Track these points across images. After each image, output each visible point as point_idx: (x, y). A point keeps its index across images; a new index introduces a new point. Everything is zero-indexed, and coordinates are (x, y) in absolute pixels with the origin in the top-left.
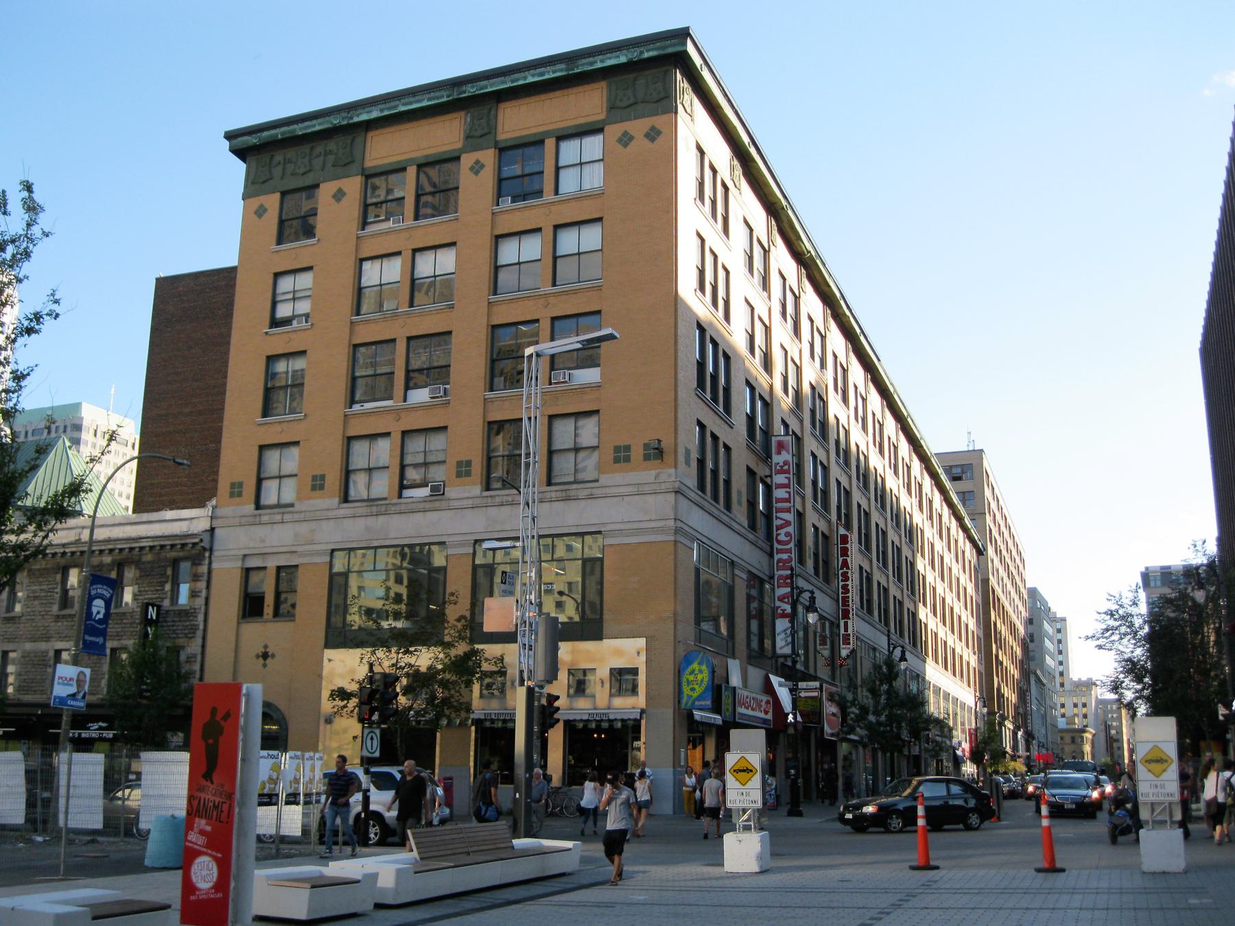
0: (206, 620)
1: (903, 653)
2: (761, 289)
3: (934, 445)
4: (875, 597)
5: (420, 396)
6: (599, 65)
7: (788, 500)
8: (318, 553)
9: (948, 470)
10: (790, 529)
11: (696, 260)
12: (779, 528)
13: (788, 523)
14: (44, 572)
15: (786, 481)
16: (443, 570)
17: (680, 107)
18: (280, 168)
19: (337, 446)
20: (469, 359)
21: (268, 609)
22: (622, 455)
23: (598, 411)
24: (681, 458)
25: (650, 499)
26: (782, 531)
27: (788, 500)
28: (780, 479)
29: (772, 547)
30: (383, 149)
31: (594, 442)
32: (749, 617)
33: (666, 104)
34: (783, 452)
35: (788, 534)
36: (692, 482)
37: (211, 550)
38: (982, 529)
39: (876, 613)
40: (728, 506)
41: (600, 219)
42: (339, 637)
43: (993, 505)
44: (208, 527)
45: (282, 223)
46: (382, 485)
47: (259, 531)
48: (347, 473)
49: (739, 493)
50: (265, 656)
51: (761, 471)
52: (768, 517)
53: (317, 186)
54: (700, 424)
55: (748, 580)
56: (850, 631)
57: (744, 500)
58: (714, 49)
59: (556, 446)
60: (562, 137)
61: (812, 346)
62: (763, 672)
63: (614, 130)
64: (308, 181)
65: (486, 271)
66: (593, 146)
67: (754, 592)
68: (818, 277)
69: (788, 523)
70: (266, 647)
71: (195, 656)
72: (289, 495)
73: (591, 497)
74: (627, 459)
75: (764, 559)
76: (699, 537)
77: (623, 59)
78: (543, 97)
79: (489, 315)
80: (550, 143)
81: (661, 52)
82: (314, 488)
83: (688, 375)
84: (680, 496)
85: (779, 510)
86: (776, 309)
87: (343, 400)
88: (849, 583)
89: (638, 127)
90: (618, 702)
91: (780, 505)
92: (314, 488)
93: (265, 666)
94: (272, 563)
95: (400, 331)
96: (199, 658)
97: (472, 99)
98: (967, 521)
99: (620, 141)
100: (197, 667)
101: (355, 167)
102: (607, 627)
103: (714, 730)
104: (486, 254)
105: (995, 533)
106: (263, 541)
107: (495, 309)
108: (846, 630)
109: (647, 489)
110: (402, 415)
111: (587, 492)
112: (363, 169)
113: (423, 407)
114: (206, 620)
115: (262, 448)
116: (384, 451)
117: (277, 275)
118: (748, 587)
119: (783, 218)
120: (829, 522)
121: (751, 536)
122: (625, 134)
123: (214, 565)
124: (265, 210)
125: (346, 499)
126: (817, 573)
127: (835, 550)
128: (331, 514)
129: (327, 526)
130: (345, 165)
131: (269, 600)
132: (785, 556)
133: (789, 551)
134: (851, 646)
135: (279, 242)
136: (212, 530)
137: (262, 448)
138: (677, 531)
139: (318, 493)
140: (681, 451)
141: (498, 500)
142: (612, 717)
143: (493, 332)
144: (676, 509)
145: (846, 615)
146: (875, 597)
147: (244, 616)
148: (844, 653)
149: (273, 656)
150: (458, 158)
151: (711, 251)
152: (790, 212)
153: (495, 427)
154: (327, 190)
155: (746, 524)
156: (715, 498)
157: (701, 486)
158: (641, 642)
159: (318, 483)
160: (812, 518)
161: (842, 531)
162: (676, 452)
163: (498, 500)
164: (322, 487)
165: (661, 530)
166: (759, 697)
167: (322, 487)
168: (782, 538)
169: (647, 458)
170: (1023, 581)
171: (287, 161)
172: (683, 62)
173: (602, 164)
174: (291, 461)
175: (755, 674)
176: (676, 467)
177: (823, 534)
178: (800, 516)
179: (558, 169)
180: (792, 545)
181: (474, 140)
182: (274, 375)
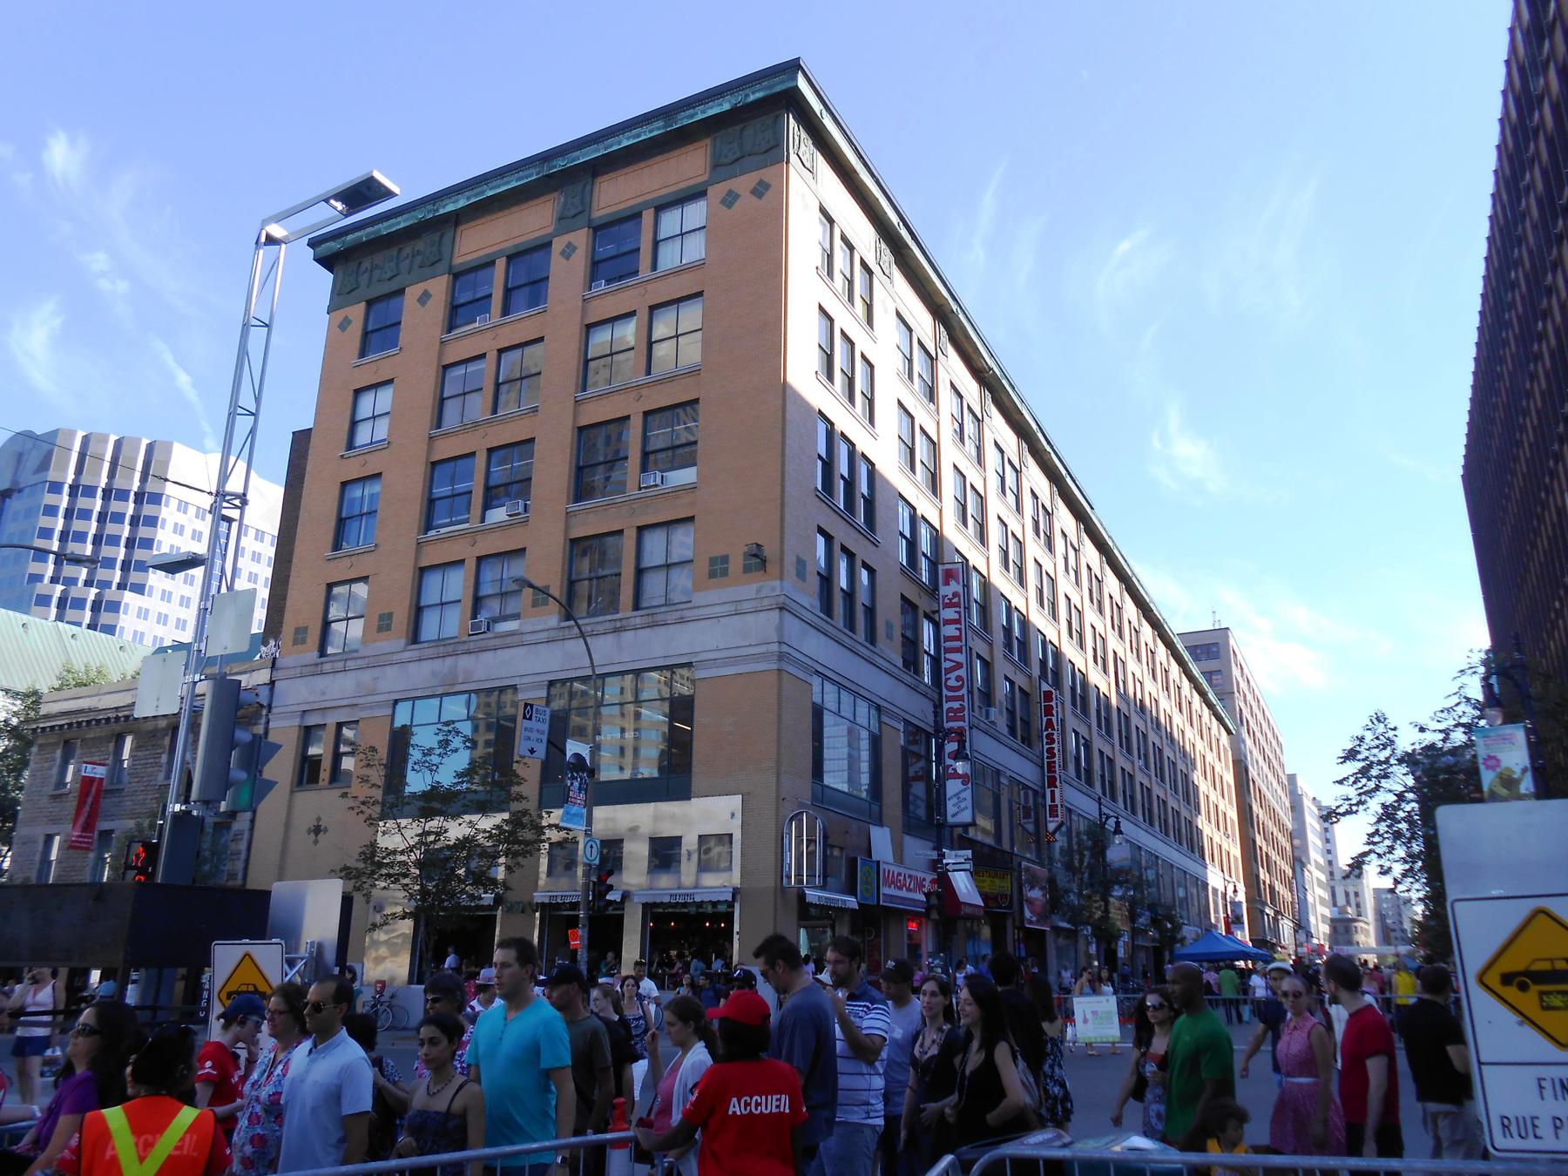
1: (1118, 823)
2: (925, 401)
3: (1177, 625)
4: (1139, 797)
5: (498, 515)
6: (700, 117)
7: (958, 638)
8: (379, 705)
9: (1192, 649)
10: (962, 672)
12: (948, 671)
13: (959, 666)
14: (97, 741)
17: (793, 158)
19: (406, 577)
20: (552, 469)
21: (325, 775)
22: (718, 568)
26: (953, 675)
27: (958, 638)
28: (949, 614)
29: (940, 694)
30: (473, 243)
33: (775, 153)
34: (953, 583)
35: (959, 678)
36: (808, 598)
37: (270, 707)
38: (1231, 709)
39: (1140, 812)
40: (872, 638)
41: (700, 294)
42: (394, 802)
43: (1243, 685)
44: (267, 680)
46: (453, 623)
47: (321, 682)
48: (418, 611)
49: (889, 625)
50: (317, 830)
51: (924, 604)
53: (401, 292)
56: (1058, 802)
58: (830, 84)
59: (646, 563)
60: (661, 207)
61: (1066, 559)
63: (717, 191)
64: (394, 285)
66: (696, 213)
68: (1007, 403)
69: (959, 666)
70: (319, 819)
71: (241, 833)
73: (682, 621)
74: (725, 573)
77: (726, 107)
78: (642, 164)
79: (575, 416)
80: (648, 216)
81: (768, 92)
85: (948, 651)
86: (994, 482)
87: (416, 525)
88: (1055, 745)
89: (743, 183)
90: (710, 880)
91: (949, 644)
93: (316, 842)
94: (331, 720)
95: (478, 443)
96: (246, 836)
97: (564, 174)
98: (1211, 696)
99: (723, 202)
100: (243, 846)
101: (443, 266)
102: (697, 780)
103: (847, 919)
105: (1246, 713)
106: (324, 693)
108: (1053, 799)
109: (746, 606)
110: (479, 538)
111: (678, 614)
112: (450, 267)
113: (500, 527)
116: (457, 584)
117: (358, 392)
119: (955, 324)
120: (1030, 677)
122: (730, 192)
123: (271, 725)
124: (350, 322)
125: (415, 638)
126: (1079, 777)
127: (1037, 710)
128: (396, 658)
129: (391, 672)
130: (431, 266)
131: (326, 764)
132: (956, 705)
133: (961, 698)
134: (1059, 819)
135: (362, 354)
136: (272, 683)
138: (781, 656)
139: (384, 634)
140: (790, 560)
142: (698, 899)
144: (780, 628)
145: (1052, 783)
146: (1139, 797)
147: (300, 782)
148: (1051, 827)
149: (326, 830)
150: (550, 244)
151: (863, 356)
152: (961, 316)
153: (578, 546)
154: (413, 293)
155: (900, 664)
158: (737, 801)
160: (1002, 668)
161: (1045, 687)
162: (782, 559)
164: (388, 628)
166: (920, 875)
167: (388, 628)
168: (952, 683)
170: (1282, 765)
172: (793, 102)
173: (703, 233)
175: (919, 850)
179: (656, 244)
180: (964, 691)
181: (566, 222)
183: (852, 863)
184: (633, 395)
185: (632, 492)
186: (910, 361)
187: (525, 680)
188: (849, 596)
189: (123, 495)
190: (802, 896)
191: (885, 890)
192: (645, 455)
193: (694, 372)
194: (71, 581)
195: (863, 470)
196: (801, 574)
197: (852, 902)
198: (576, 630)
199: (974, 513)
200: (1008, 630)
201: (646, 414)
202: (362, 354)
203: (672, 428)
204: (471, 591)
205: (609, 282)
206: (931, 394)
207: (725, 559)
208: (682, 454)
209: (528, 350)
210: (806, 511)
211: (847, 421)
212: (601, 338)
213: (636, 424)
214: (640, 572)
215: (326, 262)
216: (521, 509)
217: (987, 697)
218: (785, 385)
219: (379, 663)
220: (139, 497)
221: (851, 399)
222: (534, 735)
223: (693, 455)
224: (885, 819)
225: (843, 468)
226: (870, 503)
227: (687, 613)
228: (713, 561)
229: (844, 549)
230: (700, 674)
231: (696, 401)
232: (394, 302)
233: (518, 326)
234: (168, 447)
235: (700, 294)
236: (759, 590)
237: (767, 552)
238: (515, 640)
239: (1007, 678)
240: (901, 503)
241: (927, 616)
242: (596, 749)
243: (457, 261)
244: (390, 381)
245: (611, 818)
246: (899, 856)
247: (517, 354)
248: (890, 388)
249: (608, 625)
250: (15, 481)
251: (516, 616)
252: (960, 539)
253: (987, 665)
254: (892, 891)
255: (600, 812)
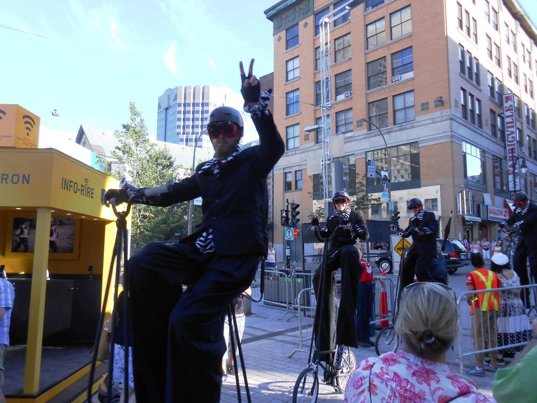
0: (273, 193)
5: (341, 97)
11: (456, 14)
12: (508, 135)
13: (513, 133)
15: (511, 114)
16: (354, 166)
18: (284, 20)
20: (358, 79)
21: (293, 187)
22: (425, 107)
23: (413, 90)
24: (453, 104)
25: (439, 124)
26: (510, 137)
28: (508, 113)
29: (505, 144)
31: (413, 104)
32: (495, 175)
34: (509, 101)
35: (513, 137)
36: (459, 115)
40: (480, 126)
41: (409, 5)
45: (287, 41)
49: (486, 120)
51: (498, 111)
52: (503, 132)
53: (297, 24)
54: (462, 89)
55: (493, 159)
57: (489, 123)
62: (504, 199)
64: (294, 23)
65: (362, 40)
67: (497, 164)
69: (513, 133)
70: (293, 201)
72: (297, 144)
73: (412, 127)
74: (427, 108)
75: (502, 149)
76: (465, 139)
82: (305, 140)
83: (457, 67)
84: (453, 122)
92: (305, 140)
94: (293, 170)
101: (311, 12)
102: (422, 182)
104: (362, 34)
106: (290, 162)
107: (368, 56)
109: (437, 120)
111: (411, 125)
112: (314, 12)
113: (343, 101)
114: (273, 193)
115: (287, 127)
117: (287, 62)
118: (493, 162)
121: (493, 139)
123: (274, 173)
128: (312, 148)
130: (306, 13)
131: (293, 184)
133: (514, 145)
135: (287, 49)
137: (287, 127)
138: (452, 136)
140: (453, 100)
141: (374, 134)
143: (368, 66)
144: (451, 127)
147: (286, 190)
154: (301, 24)
155: (491, 134)
156: (473, 122)
157: (465, 116)
158: (438, 187)
159: (307, 138)
160: (526, 132)
163: (374, 134)
164: (308, 139)
165: (445, 137)
167: (308, 139)
168: (510, 139)
169: (436, 106)
171: (286, 17)
174: (297, 130)
175: (499, 200)
176: (450, 108)
177: (533, 139)
178: (520, 131)
180: (515, 142)
182: (290, 99)
183: (478, 206)
184: (386, 48)
185: (389, 83)
186: (489, 15)
187: (357, 152)
188: (473, 111)
189: (189, 105)
190: (463, 219)
191: (490, 215)
192: (393, 69)
193: (410, 36)
194: (188, 133)
195: (474, 62)
196: (456, 106)
197: (479, 220)
198: (379, 133)
199: (514, 73)
200: (528, 117)
201: (392, 54)
202: (287, 49)
203: (403, 58)
204: (335, 124)
205: (373, 7)
206: (497, 27)
207: (427, 104)
208: (407, 67)
209: (345, 38)
210: (457, 81)
211: (469, 45)
212: (371, 28)
213: (389, 58)
214: (395, 111)
215: (271, 18)
216: (349, 94)
217: (521, 143)
218: (447, 37)
219: (306, 151)
220: (203, 104)
221: (469, 35)
222: (372, 170)
223: (412, 67)
224: (488, 190)
225: (468, 64)
226: (477, 75)
227: (414, 124)
228: (423, 105)
229: (470, 94)
230: (420, 145)
231: (411, 47)
232: (295, 28)
233: (340, 30)
234: (208, 87)
235: (409, 5)
236: (441, 113)
237: (443, 99)
238: (352, 139)
239: (528, 136)
240: (488, 73)
241: (499, 116)
242: (390, 174)
243: (316, 9)
244: (298, 56)
245: (396, 195)
246: (493, 204)
247: (341, 40)
248: (484, 27)
249: (385, 131)
250: (169, 105)
251: (352, 131)
252: (509, 84)
253: (520, 131)
254: (492, 215)
255: (393, 193)
